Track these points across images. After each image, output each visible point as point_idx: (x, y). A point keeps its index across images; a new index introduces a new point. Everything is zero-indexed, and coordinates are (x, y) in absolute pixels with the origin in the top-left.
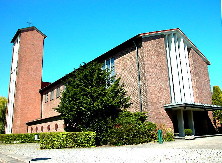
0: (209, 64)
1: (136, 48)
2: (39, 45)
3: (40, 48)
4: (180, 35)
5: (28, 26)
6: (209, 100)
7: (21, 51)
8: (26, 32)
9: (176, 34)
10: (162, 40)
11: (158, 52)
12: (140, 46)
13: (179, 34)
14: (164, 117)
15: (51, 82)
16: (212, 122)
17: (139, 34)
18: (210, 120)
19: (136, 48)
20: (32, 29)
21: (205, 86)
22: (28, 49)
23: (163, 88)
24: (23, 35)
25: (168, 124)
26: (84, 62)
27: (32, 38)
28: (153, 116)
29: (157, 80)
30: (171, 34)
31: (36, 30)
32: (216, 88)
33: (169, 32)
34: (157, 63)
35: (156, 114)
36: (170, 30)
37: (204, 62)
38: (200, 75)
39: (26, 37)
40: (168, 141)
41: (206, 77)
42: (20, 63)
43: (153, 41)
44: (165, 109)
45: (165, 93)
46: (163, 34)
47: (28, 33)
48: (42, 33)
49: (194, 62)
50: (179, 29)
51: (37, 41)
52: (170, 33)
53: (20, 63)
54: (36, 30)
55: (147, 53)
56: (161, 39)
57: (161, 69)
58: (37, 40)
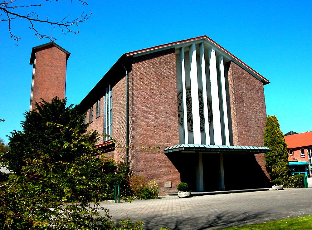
0: (265, 83)
1: (126, 71)
2: (59, 66)
3: (62, 70)
4: (209, 44)
5: (47, 41)
6: (259, 137)
7: (36, 76)
8: (43, 50)
9: (203, 44)
10: (172, 57)
11: (161, 74)
12: (130, 69)
13: (207, 43)
14: (163, 165)
15: (186, 105)
16: (264, 169)
17: (126, 54)
18: (259, 167)
19: (126, 71)
20: (51, 45)
21: (253, 117)
22: (46, 72)
23: (166, 125)
24: (38, 54)
25: (170, 174)
26: (41, 99)
27: (51, 57)
28: (142, 163)
29: (155, 114)
30: (191, 45)
31: (57, 46)
32: (271, 119)
33: (188, 43)
34: (158, 90)
35: (148, 161)
36: (188, 40)
37: (257, 81)
38: (245, 100)
39: (42, 57)
40: (144, 198)
41: (257, 102)
42: (35, 91)
43: (152, 60)
44: (166, 154)
45: (168, 131)
46: (174, 47)
47: (46, 51)
48: (64, 50)
49: (234, 82)
50: (205, 36)
51: (58, 61)
52: (191, 44)
53: (35, 91)
54: (57, 46)
55: (140, 78)
56: (169, 55)
57: (165, 98)
58: (57, 59)
